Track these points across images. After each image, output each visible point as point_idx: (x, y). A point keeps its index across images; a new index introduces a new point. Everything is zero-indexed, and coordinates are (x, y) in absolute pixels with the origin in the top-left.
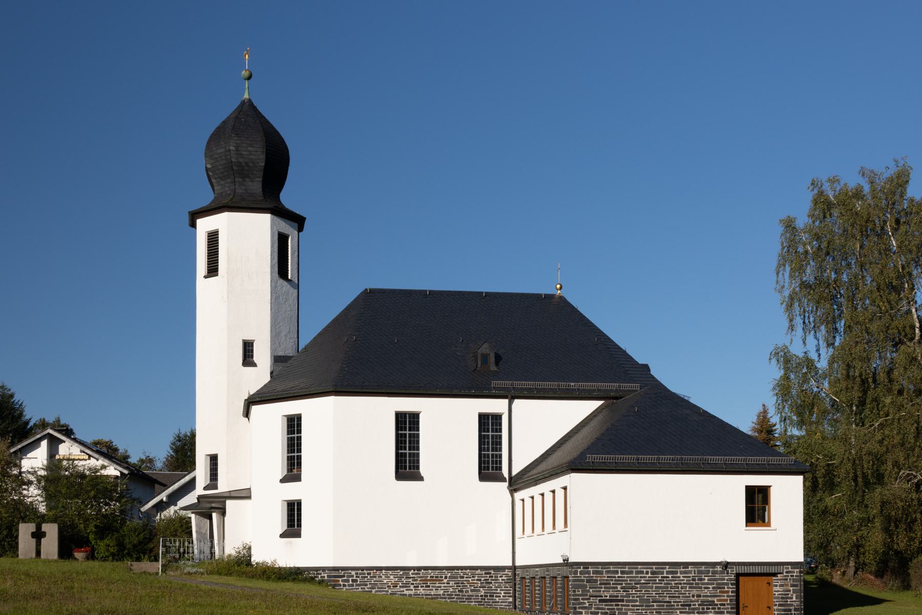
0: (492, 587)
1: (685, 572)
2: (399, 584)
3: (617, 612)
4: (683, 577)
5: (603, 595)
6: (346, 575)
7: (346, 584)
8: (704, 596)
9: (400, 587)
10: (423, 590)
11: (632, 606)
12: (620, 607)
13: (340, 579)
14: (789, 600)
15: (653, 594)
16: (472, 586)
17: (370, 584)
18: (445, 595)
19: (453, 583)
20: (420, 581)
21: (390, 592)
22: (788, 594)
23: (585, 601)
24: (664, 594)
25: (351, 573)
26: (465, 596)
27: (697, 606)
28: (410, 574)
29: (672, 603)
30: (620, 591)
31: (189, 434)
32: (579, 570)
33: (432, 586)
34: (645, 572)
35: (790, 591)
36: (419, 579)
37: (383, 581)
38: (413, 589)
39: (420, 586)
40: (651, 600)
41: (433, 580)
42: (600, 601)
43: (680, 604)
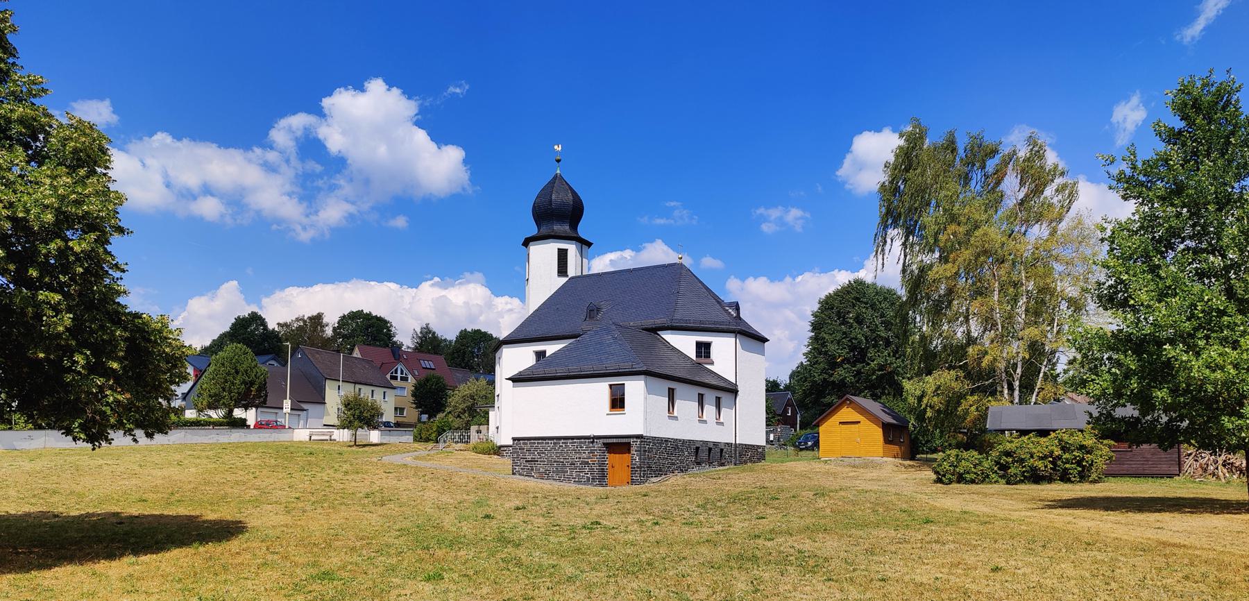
31: (1176, 130)
42: (526, 461)
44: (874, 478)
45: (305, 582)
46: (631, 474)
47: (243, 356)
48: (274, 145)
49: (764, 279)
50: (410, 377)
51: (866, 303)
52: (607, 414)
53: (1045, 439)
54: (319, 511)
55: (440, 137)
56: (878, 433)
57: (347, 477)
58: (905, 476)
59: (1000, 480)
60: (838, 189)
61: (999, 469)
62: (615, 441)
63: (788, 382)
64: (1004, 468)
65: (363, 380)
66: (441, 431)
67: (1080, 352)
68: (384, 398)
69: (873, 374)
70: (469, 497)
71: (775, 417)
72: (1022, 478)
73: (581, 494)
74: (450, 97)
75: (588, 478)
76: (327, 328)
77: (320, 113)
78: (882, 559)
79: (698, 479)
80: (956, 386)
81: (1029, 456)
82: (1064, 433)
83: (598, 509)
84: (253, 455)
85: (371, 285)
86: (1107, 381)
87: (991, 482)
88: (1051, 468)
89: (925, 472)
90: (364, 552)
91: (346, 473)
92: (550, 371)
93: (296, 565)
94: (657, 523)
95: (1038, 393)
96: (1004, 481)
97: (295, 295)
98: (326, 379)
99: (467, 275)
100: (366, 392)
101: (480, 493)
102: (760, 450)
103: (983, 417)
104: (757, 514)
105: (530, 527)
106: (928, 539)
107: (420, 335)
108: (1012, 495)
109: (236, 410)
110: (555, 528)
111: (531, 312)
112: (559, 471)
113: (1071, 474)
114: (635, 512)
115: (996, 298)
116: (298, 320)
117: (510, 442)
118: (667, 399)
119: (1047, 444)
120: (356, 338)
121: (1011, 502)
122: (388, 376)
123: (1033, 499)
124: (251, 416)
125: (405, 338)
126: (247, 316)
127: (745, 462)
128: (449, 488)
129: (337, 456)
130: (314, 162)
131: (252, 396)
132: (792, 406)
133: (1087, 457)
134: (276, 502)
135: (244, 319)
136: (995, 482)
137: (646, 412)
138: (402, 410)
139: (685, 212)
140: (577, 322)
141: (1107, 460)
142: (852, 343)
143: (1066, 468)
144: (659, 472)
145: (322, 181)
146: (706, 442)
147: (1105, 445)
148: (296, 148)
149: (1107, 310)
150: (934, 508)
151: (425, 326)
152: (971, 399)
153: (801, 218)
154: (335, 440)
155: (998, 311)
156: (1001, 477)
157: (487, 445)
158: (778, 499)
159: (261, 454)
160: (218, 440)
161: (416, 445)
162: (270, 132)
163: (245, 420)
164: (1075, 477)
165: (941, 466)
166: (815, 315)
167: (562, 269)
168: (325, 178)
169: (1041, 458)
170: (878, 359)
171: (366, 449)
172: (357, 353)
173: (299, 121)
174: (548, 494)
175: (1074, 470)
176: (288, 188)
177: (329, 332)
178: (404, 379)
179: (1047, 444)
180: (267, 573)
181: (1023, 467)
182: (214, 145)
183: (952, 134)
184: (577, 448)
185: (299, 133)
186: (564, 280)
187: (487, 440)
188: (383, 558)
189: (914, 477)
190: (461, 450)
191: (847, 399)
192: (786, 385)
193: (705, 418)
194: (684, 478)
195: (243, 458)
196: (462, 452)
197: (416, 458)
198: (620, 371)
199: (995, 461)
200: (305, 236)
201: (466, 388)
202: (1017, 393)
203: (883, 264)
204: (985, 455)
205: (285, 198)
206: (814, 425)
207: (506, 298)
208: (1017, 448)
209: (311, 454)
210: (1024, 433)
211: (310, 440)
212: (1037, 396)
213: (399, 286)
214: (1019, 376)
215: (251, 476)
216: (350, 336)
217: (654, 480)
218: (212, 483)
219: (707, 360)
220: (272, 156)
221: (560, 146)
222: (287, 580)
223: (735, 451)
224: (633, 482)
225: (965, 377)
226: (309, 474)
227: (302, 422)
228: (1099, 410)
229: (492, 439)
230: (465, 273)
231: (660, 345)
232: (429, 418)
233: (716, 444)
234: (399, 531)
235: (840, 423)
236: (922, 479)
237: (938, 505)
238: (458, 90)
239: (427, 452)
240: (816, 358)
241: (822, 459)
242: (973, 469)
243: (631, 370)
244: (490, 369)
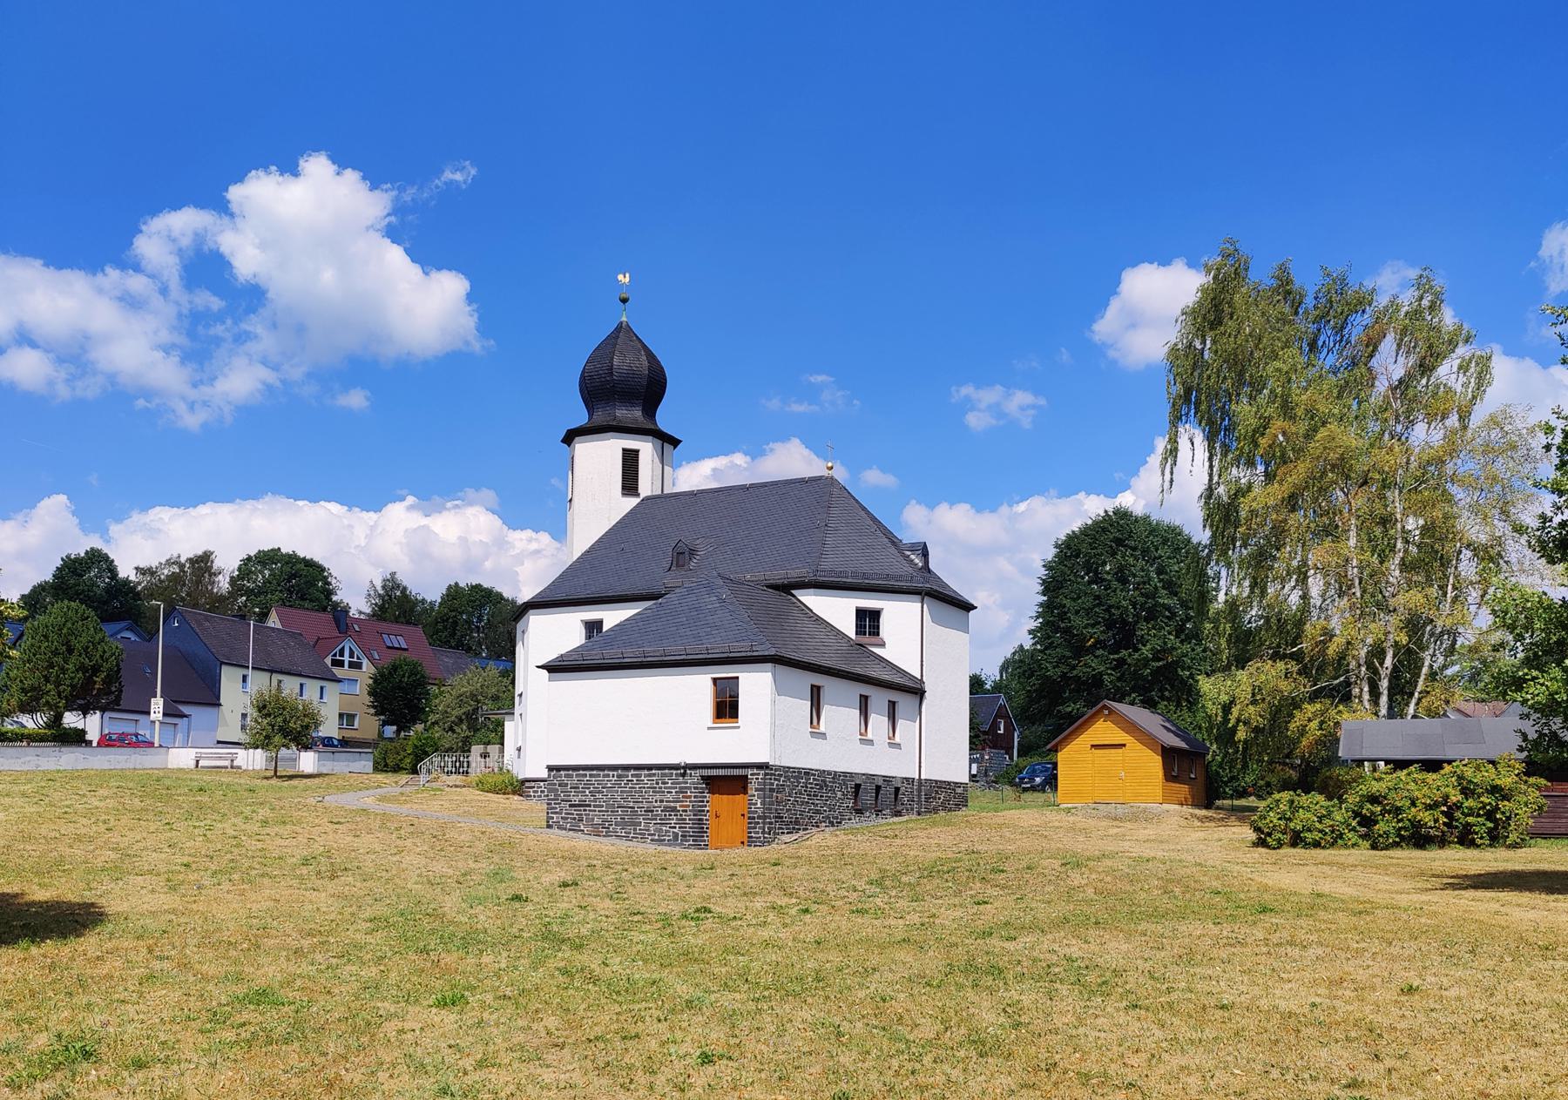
1: (650, 775)
8: (667, 801)
11: (599, 811)
13: (531, 790)
35: (754, 796)
42: (570, 806)
44: (1151, 838)
45: (229, 1009)
46: (749, 828)
47: (80, 623)
48: (143, 263)
49: (967, 506)
50: (365, 662)
51: (1134, 549)
52: (709, 728)
53: (1434, 776)
54: (226, 886)
55: (428, 256)
56: (1155, 763)
57: (268, 830)
58: (1201, 835)
59: (1360, 841)
60: (1094, 355)
61: (1359, 824)
62: (721, 772)
63: (998, 678)
64: (1367, 822)
65: (285, 667)
66: (420, 754)
67: (1511, 633)
68: (321, 698)
69: (1146, 666)
70: (480, 865)
71: (981, 737)
72: (1397, 840)
73: (667, 861)
74: (445, 187)
76: (220, 577)
77: (221, 206)
78: (1210, 972)
79: (860, 838)
80: (1285, 687)
81: (1408, 803)
82: (1465, 765)
83: (701, 887)
84: (101, 792)
85: (298, 505)
86: (1557, 681)
87: (1346, 846)
88: (1444, 824)
89: (1234, 829)
90: (319, 957)
91: (265, 823)
92: (612, 655)
93: (206, 979)
94: (806, 911)
95: (1420, 700)
96: (1367, 844)
97: (167, 520)
98: (222, 663)
99: (470, 492)
100: (290, 685)
101: (496, 859)
102: (959, 790)
103: (1330, 741)
104: (972, 896)
105: (592, 915)
106: (1275, 938)
107: (381, 592)
108: (1386, 867)
109: (67, 714)
110: (636, 918)
111: (577, 554)
112: (628, 823)
113: (1477, 833)
114: (765, 892)
115: (1352, 542)
116: (169, 563)
117: (544, 774)
118: (809, 703)
119: (1440, 784)
120: (269, 596)
121: (1387, 879)
122: (328, 661)
123: (1422, 874)
124: (92, 725)
125: (356, 598)
126: (82, 555)
127: (936, 810)
128: (442, 850)
129: (246, 794)
130: (209, 293)
131: (95, 692)
132: (1006, 717)
133: (1504, 806)
134: (150, 872)
135: (78, 560)
136: (1354, 845)
137: (774, 724)
138: (351, 717)
139: (839, 394)
140: (656, 573)
141: (1535, 810)
142: (1112, 615)
143: (1468, 824)
144: (795, 826)
145: (223, 327)
146: (870, 777)
147: (1532, 785)
148: (178, 267)
149: (1554, 563)
150: (1266, 889)
151: (389, 577)
152: (1310, 708)
153: (1033, 407)
154: (239, 767)
155: (1354, 564)
156: (1364, 837)
157: (501, 778)
158: (1003, 871)
159: (115, 790)
160: (38, 766)
161: (380, 777)
162: (135, 240)
163: (83, 732)
164: (1482, 838)
165: (1265, 818)
166: (1048, 566)
167: (630, 484)
168: (229, 322)
169: (1429, 807)
170: (1153, 639)
171: (295, 782)
172: (274, 621)
173: (184, 221)
174: (613, 861)
175: (1481, 825)
176: (165, 336)
177: (223, 584)
178: (356, 666)
179: (1440, 784)
180: (157, 993)
181: (1399, 821)
182: (38, 263)
183: (1283, 268)
184: (657, 783)
185: (185, 242)
186: (632, 502)
187: (501, 769)
188: (354, 968)
189: (1216, 836)
190: (456, 786)
191: (1105, 707)
192: (995, 682)
193: (870, 736)
194: (836, 835)
195: (84, 795)
196: (458, 789)
197: (382, 799)
198: (731, 655)
199: (1353, 811)
200: (192, 421)
201: (465, 682)
202: (1384, 699)
203: (1172, 481)
204: (1336, 801)
205: (159, 355)
206: (1050, 750)
207: (529, 533)
208: (1389, 789)
209: (201, 790)
210: (1400, 765)
211: (197, 766)
212: (1417, 704)
213: (346, 508)
214: (1388, 672)
215: (102, 827)
216: (259, 592)
217: (786, 838)
218: (35, 838)
219: (873, 639)
220: (137, 283)
221: (627, 275)
222: (194, 1004)
223: (919, 791)
224: (751, 842)
225: (1299, 673)
226: (202, 824)
227: (179, 736)
228: (1536, 728)
229: (510, 767)
230: (467, 489)
231: (795, 612)
232: (398, 732)
233: (887, 780)
234: (371, 921)
235: (1093, 746)
236: (1231, 840)
237: (1270, 883)
238: (458, 177)
239: (399, 790)
240: (1049, 637)
241: (1061, 806)
242: (1317, 825)
243: (749, 654)
244: (505, 650)
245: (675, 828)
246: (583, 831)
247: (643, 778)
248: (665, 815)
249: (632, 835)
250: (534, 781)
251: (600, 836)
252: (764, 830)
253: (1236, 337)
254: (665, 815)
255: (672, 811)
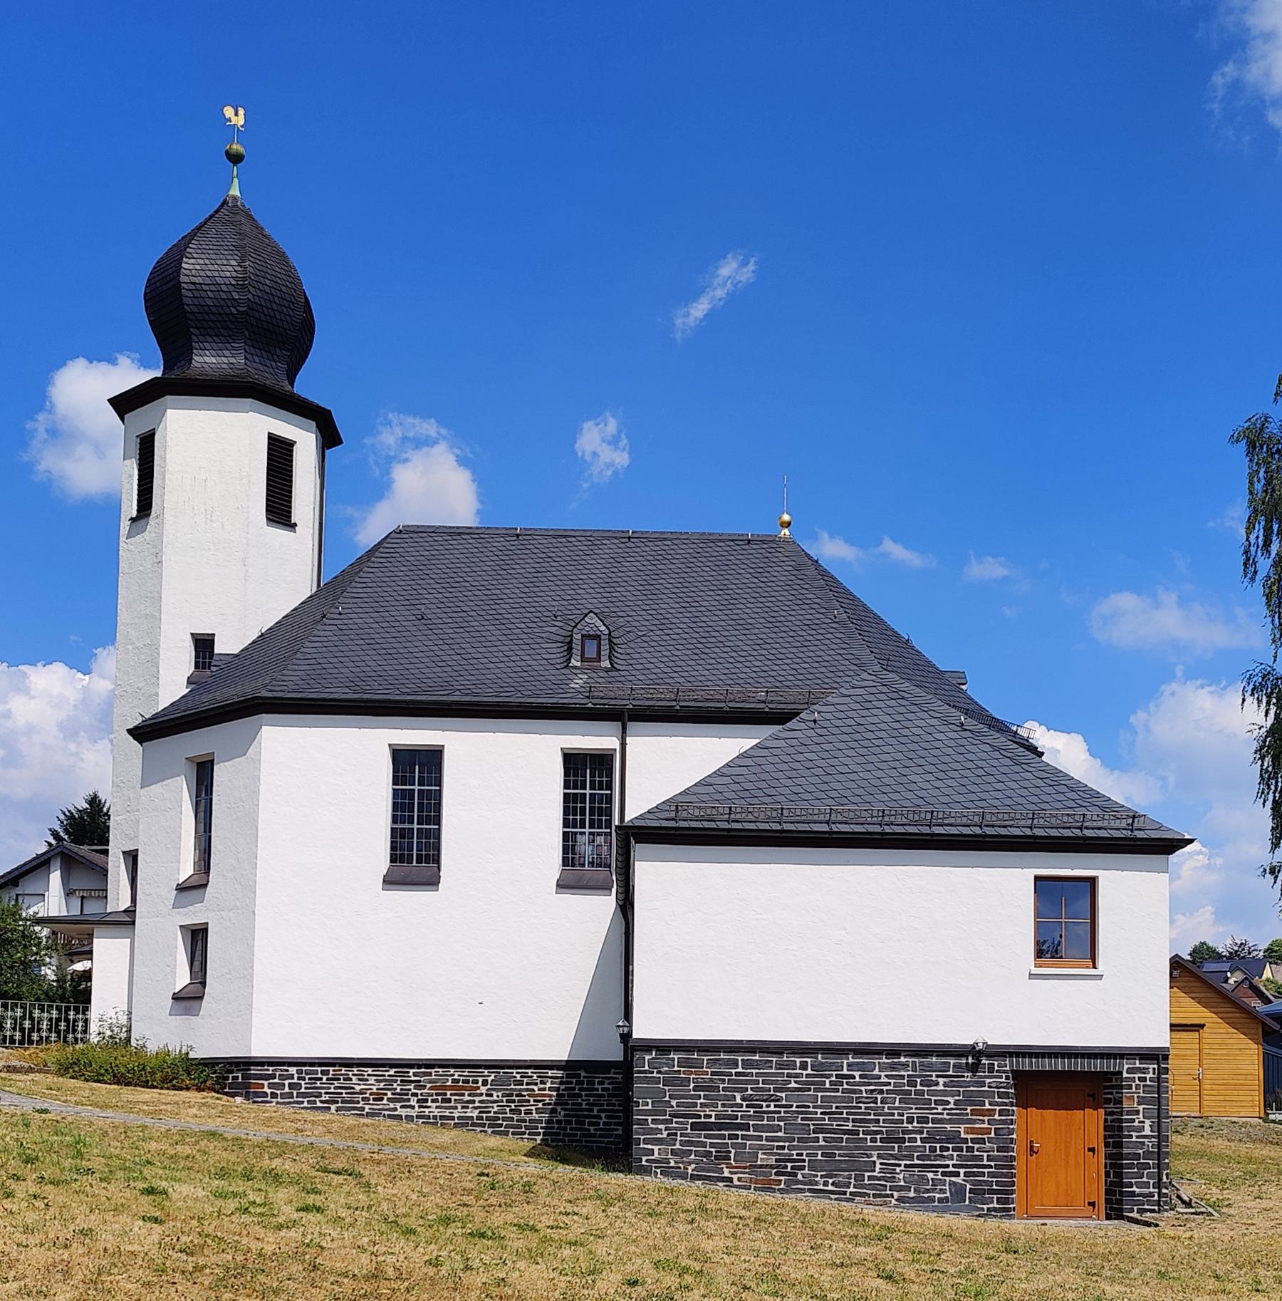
0: (581, 1104)
1: (893, 1067)
2: (386, 1094)
3: (733, 1151)
4: (886, 1076)
5: (702, 1114)
6: (277, 1073)
7: (278, 1092)
8: (934, 1121)
9: (389, 1099)
10: (437, 1107)
11: (768, 1139)
12: (740, 1141)
13: (266, 1083)
14: (1134, 1134)
15: (816, 1113)
16: (540, 1101)
17: (326, 1093)
18: (482, 1118)
19: (500, 1094)
20: (431, 1088)
21: (367, 1110)
22: (1133, 1120)
23: (660, 1126)
24: (842, 1113)
25: (287, 1071)
26: (525, 1121)
27: (919, 1143)
28: (411, 1074)
29: (861, 1136)
30: (741, 1106)
32: (647, 1057)
33: (455, 1100)
34: (798, 1064)
35: (1137, 1112)
36: (429, 1085)
37: (353, 1088)
38: (417, 1105)
39: (430, 1098)
40: (812, 1127)
41: (457, 1088)
43: (878, 1137)
52: (1032, 976)
62: (1060, 1065)
75: (958, 1192)
221: (241, 112)
245: (957, 1174)
246: (730, 1180)
247: (876, 1072)
248: (933, 1149)
249: (852, 1189)
250: (271, 1064)
251: (774, 1190)
252: (1160, 1179)
253: (188, 502)
254: (933, 1149)
255: (948, 1141)
